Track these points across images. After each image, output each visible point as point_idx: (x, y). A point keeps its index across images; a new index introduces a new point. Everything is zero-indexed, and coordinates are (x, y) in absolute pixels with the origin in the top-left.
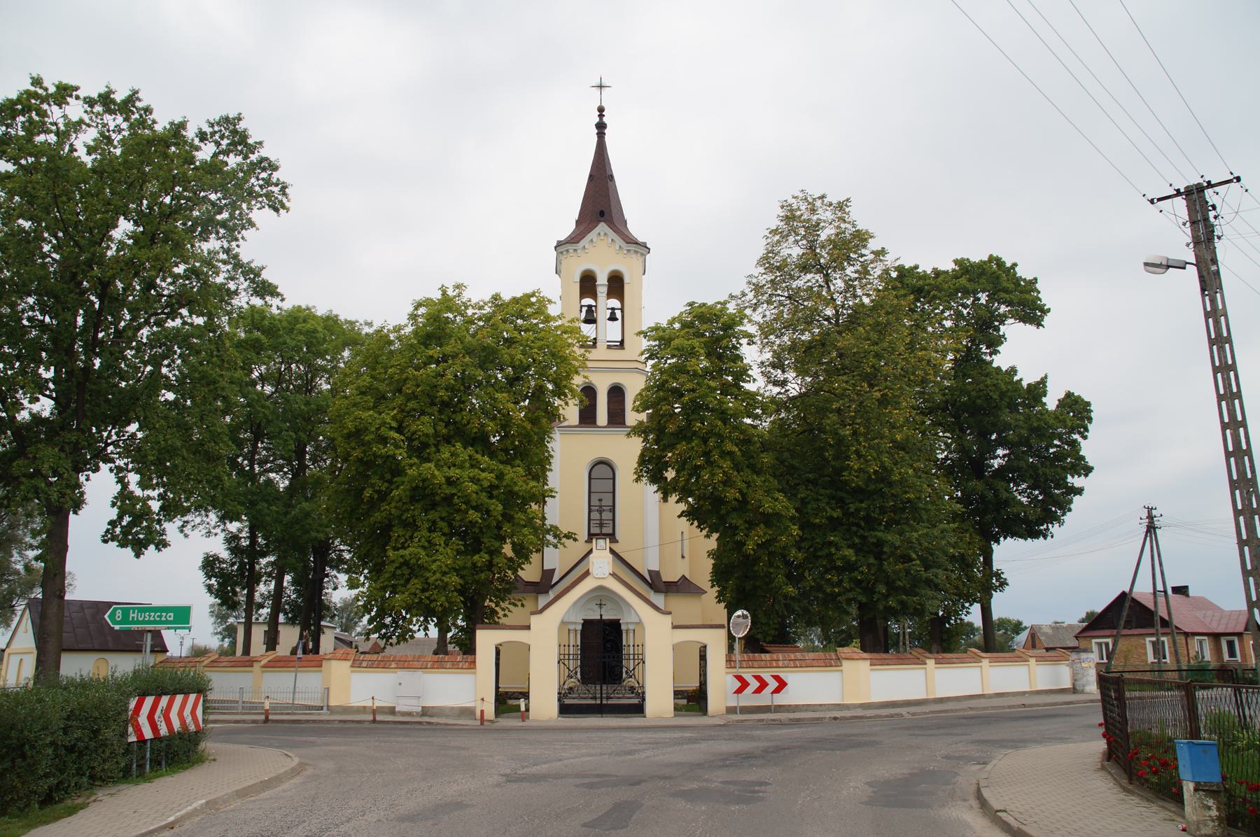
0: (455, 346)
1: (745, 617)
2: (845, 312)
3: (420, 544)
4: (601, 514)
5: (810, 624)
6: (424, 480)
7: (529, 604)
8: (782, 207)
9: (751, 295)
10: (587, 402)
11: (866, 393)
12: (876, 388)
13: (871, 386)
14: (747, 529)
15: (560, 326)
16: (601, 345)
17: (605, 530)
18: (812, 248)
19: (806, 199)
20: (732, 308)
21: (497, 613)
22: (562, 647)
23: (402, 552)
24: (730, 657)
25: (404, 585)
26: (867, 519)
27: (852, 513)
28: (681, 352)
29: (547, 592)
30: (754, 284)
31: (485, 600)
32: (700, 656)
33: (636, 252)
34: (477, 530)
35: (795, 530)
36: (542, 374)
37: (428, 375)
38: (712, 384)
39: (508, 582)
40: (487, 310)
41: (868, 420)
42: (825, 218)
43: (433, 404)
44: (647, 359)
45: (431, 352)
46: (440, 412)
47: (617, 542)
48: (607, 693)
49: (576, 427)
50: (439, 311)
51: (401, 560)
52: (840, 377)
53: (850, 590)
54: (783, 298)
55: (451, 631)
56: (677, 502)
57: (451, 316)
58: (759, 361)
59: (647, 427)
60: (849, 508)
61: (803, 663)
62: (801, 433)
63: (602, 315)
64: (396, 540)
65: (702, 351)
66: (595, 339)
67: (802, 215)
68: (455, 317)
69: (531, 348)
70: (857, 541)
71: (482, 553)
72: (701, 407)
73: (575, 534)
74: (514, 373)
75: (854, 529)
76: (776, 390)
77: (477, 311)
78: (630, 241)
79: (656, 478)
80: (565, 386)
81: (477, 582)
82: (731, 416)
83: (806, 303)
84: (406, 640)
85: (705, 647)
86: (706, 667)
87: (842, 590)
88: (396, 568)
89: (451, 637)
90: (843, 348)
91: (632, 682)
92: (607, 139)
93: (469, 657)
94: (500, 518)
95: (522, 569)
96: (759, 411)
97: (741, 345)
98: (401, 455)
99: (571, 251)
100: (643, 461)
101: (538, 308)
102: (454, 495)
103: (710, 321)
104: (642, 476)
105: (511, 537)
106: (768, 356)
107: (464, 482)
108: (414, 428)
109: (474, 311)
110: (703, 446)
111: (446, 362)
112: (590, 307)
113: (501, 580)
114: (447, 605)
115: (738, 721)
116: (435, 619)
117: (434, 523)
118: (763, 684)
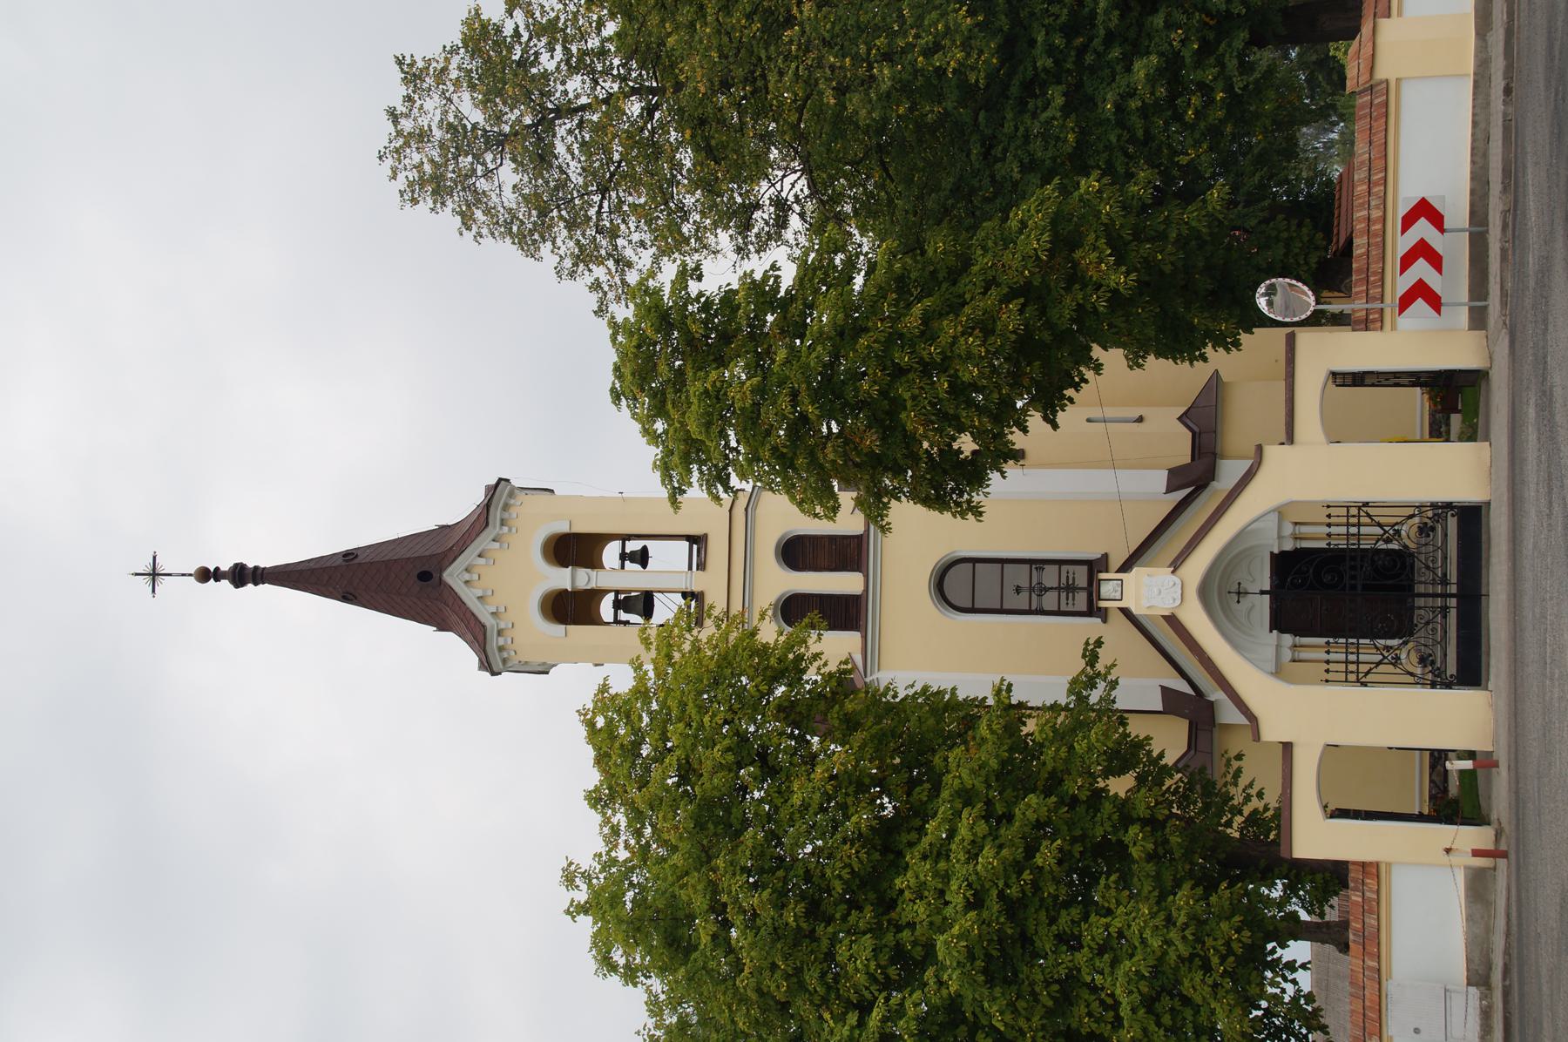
0: (694, 887)
1: (1271, 291)
2: (634, 75)
3: (1107, 970)
4: (1047, 590)
5: (1290, 150)
6: (971, 957)
7: (1234, 744)
8: (414, 201)
9: (599, 272)
10: (814, 615)
11: (803, 32)
12: (795, 11)
13: (790, 21)
14: (1084, 287)
15: (656, 669)
16: (697, 582)
17: (1082, 581)
18: (498, 142)
19: (397, 151)
20: (624, 312)
21: (1256, 811)
22: (1330, 676)
23: (1125, 1011)
24: (1358, 322)
25: (1197, 1010)
26: (1069, 31)
27: (1056, 62)
28: (715, 420)
29: (1211, 705)
30: (575, 265)
31: (1228, 836)
32: (1354, 385)
33: (506, 507)
34: (1078, 848)
35: (1089, 184)
36: (750, 705)
37: (753, 946)
38: (781, 355)
39: (1190, 787)
40: (620, 818)
41: (860, 29)
42: (438, 112)
43: (812, 936)
44: (727, 488)
45: (705, 939)
46: (829, 920)
47: (1105, 556)
48: (1434, 583)
49: (865, 638)
50: (620, 921)
51: (1142, 1012)
52: (771, 86)
53: (1221, 64)
54: (606, 204)
55: (1295, 912)
56: (1025, 430)
57: (630, 895)
58: (734, 257)
59: (868, 489)
60: (1045, 69)
61: (1378, 164)
62: (886, 170)
63: (634, 579)
64: (1097, 1021)
65: (714, 375)
66: (685, 595)
67: (432, 161)
68: (631, 884)
69: (701, 726)
70: (1116, 53)
71: (1127, 839)
72: (828, 380)
73: (1087, 643)
74: (751, 764)
75: (1089, 58)
76: (795, 222)
77: (621, 841)
78: (483, 518)
79: (973, 473)
80: (780, 660)
81: (1188, 854)
82: (847, 316)
83: (616, 157)
84: (1316, 1011)
85: (1334, 374)
86: (1378, 374)
87: (1220, 84)
88: (1159, 1025)
89: (1309, 913)
90: (710, 80)
91: (1409, 530)
92: (267, 562)
93: (1352, 875)
94: (1054, 799)
95: (1161, 756)
96: (839, 259)
97: (701, 294)
98: (916, 1004)
99: (501, 641)
100: (937, 501)
101: (618, 712)
102: (1001, 895)
103: (650, 359)
104: (969, 502)
105: (1093, 777)
106: (724, 239)
107: (977, 874)
108: (861, 978)
109: (621, 846)
110: (911, 376)
111: (725, 905)
112: (618, 605)
113: (1184, 801)
114: (1237, 918)
115: (1504, 304)
116: (1269, 946)
117: (1061, 938)
118: (1423, 250)
